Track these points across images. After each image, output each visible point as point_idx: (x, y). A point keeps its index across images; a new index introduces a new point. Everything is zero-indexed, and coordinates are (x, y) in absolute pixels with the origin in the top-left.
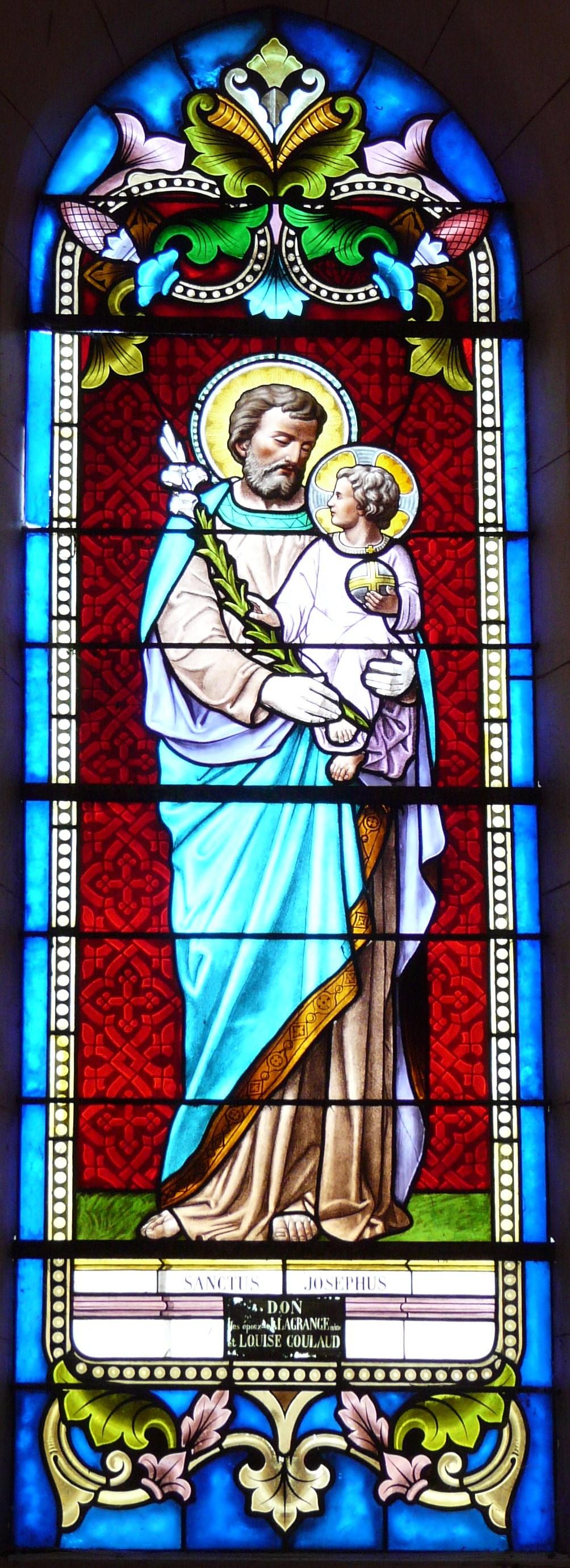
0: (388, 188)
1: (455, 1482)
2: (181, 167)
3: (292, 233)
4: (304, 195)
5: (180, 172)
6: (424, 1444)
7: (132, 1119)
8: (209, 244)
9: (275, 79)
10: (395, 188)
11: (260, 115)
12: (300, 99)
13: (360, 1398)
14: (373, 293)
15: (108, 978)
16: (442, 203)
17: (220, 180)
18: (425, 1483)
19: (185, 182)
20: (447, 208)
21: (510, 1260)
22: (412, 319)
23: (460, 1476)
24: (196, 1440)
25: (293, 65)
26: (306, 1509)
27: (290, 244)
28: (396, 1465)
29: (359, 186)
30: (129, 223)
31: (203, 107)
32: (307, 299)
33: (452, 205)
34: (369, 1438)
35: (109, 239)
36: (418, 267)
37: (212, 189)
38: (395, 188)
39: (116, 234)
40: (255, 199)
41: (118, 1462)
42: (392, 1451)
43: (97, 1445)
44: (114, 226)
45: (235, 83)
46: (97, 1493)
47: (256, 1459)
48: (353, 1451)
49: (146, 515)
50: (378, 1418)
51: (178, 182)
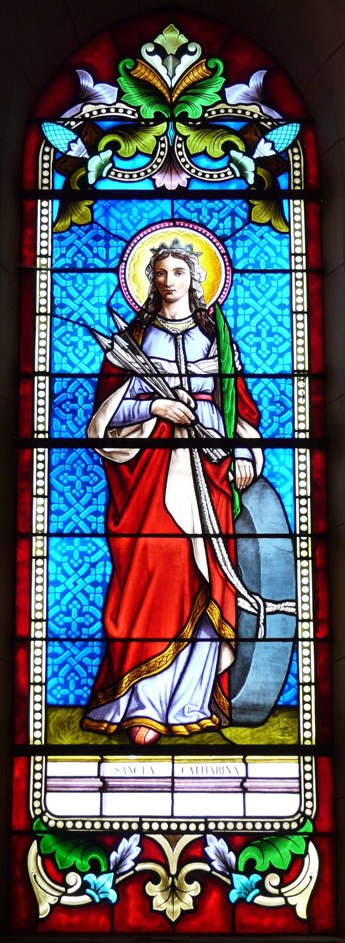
0: (240, 112)
1: (276, 891)
2: (115, 101)
3: (180, 139)
4: (189, 117)
5: (114, 104)
6: (256, 868)
7: (81, 477)
8: (131, 147)
9: (171, 50)
10: (244, 112)
11: (162, 71)
12: (187, 61)
13: (218, 840)
14: (230, 173)
15: (69, 393)
16: (271, 119)
17: (138, 108)
18: (257, 891)
19: (117, 110)
20: (274, 123)
21: (308, 755)
22: (254, 188)
23: (279, 887)
24: (119, 865)
25: (183, 40)
26: (185, 908)
27: (179, 146)
28: (239, 880)
29: (222, 111)
30: (83, 134)
31: (128, 67)
32: (189, 177)
33: (277, 120)
34: (223, 866)
35: (71, 144)
36: (257, 158)
37: (133, 114)
38: (244, 112)
39: (75, 141)
40: (158, 119)
41: (72, 878)
42: (237, 872)
43: (60, 868)
44: (74, 137)
45: (147, 52)
46: (60, 897)
47: (154, 878)
48: (213, 873)
49: (90, 261)
50: (229, 852)
51: (113, 110)
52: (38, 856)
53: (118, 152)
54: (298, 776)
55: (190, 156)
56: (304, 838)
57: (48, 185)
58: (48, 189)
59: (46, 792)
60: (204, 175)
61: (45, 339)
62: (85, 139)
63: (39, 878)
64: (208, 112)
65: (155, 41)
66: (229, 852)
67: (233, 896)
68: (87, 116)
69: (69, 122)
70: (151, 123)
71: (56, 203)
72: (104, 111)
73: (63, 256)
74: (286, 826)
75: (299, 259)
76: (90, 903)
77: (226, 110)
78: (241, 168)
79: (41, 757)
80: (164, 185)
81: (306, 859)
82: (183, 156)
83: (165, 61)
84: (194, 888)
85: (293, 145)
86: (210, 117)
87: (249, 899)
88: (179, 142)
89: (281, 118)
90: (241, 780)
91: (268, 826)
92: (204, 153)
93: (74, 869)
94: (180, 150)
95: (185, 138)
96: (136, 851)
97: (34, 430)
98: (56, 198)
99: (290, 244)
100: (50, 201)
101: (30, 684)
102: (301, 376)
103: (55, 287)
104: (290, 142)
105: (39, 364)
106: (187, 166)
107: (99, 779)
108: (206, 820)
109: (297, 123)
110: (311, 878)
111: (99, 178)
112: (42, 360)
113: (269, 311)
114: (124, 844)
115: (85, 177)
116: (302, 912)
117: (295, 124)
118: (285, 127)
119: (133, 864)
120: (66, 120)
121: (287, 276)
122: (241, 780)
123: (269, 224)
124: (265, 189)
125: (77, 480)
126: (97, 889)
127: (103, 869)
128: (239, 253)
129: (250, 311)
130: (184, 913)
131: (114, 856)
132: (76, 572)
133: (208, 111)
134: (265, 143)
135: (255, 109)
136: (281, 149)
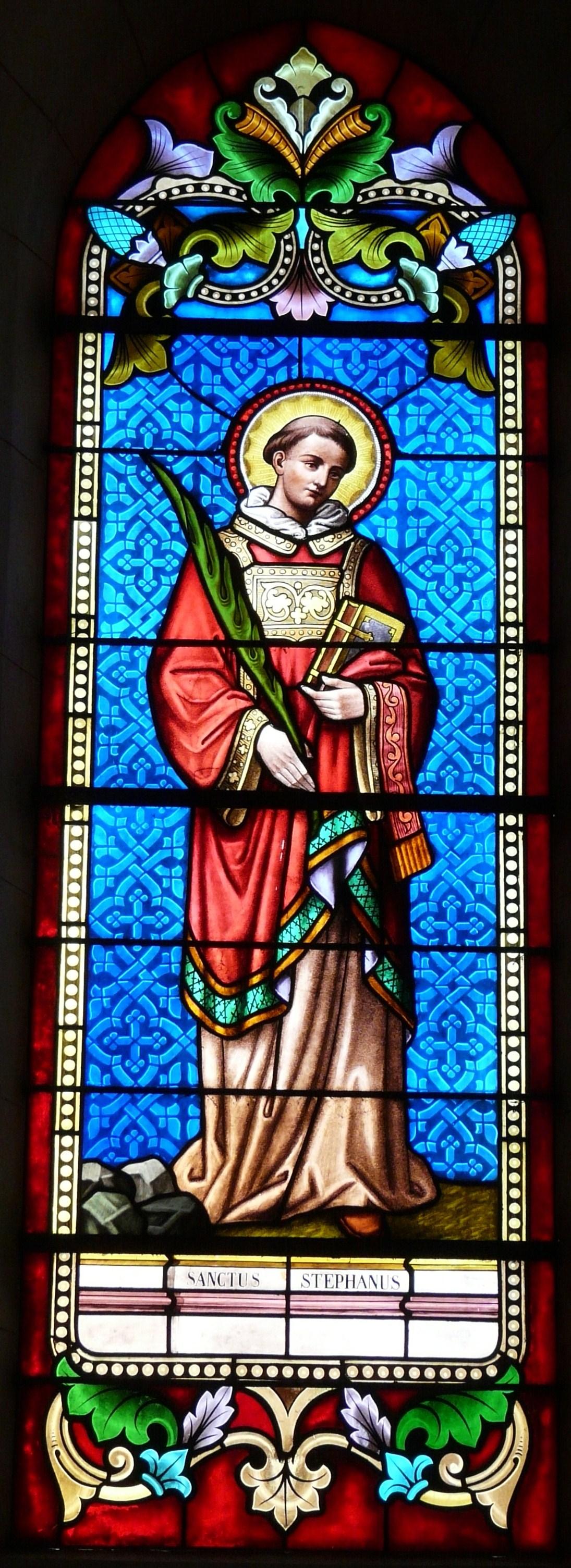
1: (458, 1483)
2: (208, 174)
3: (317, 236)
11: (289, 124)
12: (328, 108)
14: (398, 294)
16: (468, 207)
17: (247, 186)
18: (425, 1483)
19: (212, 187)
23: (461, 1476)
25: (323, 73)
28: (397, 1464)
29: (386, 192)
31: (230, 115)
32: (331, 300)
33: (477, 209)
37: (239, 195)
38: (422, 193)
40: (283, 204)
41: (120, 1456)
42: (394, 1450)
44: (140, 231)
46: (98, 1488)
47: (257, 1458)
48: (353, 1450)
51: (205, 188)
52: (64, 1419)
53: (213, 258)
54: (496, 1292)
55: (334, 268)
56: (506, 1395)
57: (97, 308)
58: (96, 315)
59: (78, 1313)
60: (354, 297)
61: (89, 547)
62: (160, 235)
63: (63, 1454)
64: (362, 194)
65: (277, 74)
66: (380, 1418)
67: (385, 1491)
68: (163, 196)
69: (131, 207)
70: (271, 211)
71: (110, 339)
72: (190, 189)
73: (121, 425)
74: (476, 1375)
75: (512, 438)
76: (148, 1497)
77: (393, 191)
78: (418, 286)
79: (69, 1255)
80: (290, 313)
81: (509, 1431)
82: (320, 265)
83: (292, 107)
84: (323, 1476)
85: (504, 250)
86: (367, 202)
87: (411, 1497)
88: (315, 240)
89: (484, 205)
90: (401, 1298)
91: (445, 1374)
92: (357, 260)
93: (121, 1440)
94: (316, 253)
95: (326, 235)
96: (226, 1413)
97: (67, 709)
98: (110, 331)
99: (497, 883)
100: (99, 335)
101: (53, 1133)
102: (512, 646)
103: (101, 699)
104: (500, 245)
105: (69, 909)
106: (328, 281)
107: (165, 1294)
108: (343, 1362)
109: (511, 213)
110: (516, 1461)
111: (182, 298)
112: (74, 902)
113: (458, 521)
114: (205, 1401)
115: (158, 298)
116: (499, 1517)
117: (507, 216)
118: (491, 222)
119: (221, 1434)
120: (126, 203)
121: (489, 466)
122: (401, 1298)
123: (463, 379)
124: (457, 321)
125: (134, 922)
126: (159, 1472)
127: (172, 1442)
128: (411, 426)
129: (426, 521)
130: (302, 1516)
131: (190, 1421)
132: (140, 497)
133: (361, 192)
134: (457, 246)
135: (440, 188)
136: (485, 257)
